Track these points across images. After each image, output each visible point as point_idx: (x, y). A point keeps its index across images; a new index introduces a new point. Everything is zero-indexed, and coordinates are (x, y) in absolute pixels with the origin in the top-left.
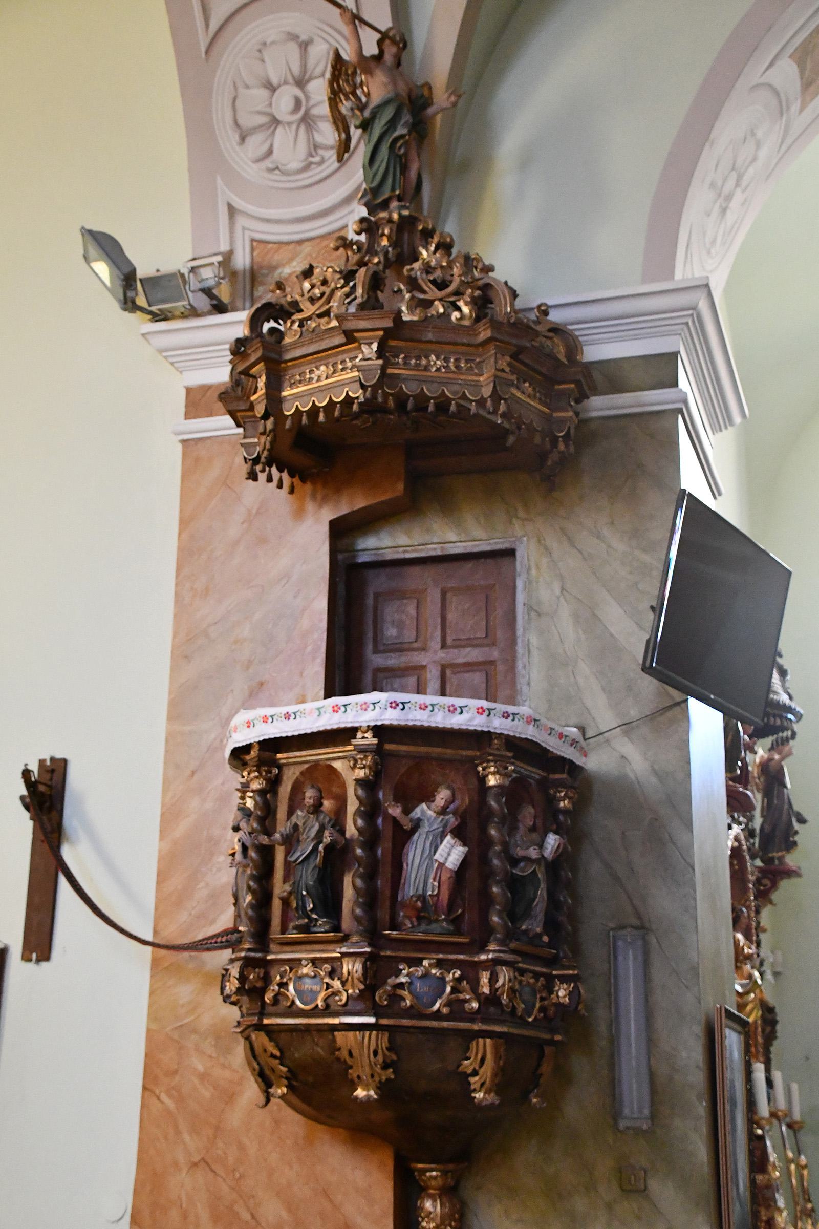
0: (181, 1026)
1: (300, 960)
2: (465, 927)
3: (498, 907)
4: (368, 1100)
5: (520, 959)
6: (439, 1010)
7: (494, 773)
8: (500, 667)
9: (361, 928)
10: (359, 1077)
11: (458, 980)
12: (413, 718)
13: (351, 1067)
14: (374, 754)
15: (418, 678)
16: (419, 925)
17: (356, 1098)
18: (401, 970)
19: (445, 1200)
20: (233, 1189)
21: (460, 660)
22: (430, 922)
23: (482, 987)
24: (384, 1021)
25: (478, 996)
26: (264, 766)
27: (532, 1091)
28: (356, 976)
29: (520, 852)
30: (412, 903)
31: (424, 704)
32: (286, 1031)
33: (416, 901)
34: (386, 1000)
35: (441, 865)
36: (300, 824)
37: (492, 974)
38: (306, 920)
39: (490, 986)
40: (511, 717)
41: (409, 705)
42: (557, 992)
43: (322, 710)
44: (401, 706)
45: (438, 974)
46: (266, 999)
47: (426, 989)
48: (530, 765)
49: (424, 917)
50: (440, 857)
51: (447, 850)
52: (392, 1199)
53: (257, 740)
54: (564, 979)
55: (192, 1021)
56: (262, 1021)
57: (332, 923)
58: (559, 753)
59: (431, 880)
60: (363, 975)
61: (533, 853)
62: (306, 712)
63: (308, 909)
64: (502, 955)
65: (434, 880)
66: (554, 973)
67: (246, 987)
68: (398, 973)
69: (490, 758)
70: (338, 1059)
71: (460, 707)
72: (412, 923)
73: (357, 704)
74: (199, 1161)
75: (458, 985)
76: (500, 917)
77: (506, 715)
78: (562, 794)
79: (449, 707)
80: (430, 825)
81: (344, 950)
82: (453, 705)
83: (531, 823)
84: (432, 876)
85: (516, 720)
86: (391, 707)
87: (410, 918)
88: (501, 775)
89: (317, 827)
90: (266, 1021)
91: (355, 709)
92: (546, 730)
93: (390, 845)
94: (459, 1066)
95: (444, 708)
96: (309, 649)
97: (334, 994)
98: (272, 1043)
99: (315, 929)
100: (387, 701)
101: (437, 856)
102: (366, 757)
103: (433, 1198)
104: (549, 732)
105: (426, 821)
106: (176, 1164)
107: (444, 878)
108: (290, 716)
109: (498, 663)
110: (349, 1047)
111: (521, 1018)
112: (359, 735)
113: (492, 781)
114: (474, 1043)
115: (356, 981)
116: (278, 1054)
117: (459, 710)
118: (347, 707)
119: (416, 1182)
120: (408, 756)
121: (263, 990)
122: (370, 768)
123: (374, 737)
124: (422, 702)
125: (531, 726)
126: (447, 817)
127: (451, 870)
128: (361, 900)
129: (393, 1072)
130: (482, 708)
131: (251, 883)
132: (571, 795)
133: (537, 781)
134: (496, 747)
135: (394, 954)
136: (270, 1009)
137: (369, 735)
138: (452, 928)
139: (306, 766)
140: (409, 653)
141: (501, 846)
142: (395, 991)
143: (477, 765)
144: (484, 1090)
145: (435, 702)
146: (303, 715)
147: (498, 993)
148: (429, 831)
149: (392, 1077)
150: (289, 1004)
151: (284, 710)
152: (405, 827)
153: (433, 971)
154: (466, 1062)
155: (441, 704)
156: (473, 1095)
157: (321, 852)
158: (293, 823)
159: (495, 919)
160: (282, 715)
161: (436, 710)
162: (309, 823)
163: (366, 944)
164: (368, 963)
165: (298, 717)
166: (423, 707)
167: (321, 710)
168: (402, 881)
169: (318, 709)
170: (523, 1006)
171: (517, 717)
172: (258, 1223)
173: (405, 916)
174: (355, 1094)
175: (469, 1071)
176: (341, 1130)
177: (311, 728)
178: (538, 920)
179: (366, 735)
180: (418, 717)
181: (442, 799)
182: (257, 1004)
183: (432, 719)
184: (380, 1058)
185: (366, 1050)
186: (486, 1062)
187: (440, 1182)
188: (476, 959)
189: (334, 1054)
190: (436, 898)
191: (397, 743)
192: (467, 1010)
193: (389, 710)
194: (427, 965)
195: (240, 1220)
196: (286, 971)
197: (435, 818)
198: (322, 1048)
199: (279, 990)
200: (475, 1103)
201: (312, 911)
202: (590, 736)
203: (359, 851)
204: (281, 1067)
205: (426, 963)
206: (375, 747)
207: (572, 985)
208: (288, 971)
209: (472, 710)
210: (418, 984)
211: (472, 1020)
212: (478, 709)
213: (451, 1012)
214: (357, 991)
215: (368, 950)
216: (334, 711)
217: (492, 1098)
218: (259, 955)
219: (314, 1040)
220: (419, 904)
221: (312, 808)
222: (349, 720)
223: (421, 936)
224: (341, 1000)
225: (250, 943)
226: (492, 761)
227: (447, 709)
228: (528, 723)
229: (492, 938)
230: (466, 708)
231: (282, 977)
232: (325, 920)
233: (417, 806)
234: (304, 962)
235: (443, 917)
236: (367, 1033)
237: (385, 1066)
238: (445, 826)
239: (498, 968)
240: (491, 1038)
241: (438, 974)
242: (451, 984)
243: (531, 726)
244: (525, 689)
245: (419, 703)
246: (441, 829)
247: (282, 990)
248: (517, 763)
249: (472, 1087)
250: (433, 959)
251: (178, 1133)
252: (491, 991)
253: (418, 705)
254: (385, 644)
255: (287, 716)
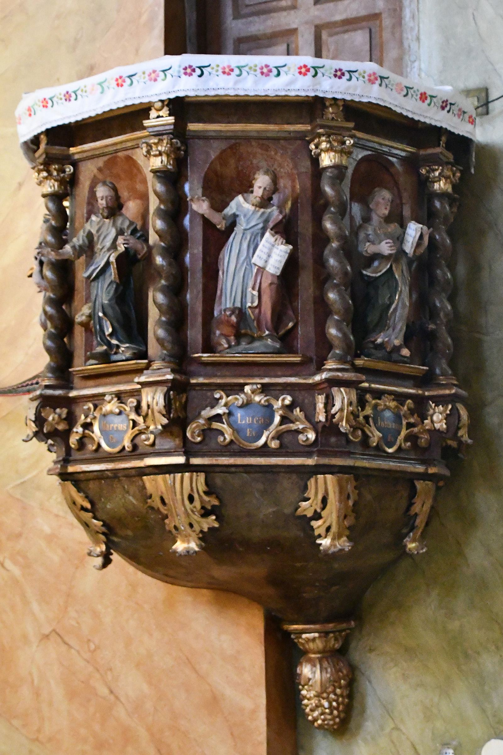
0: (22, 483)
1: (103, 395)
2: (299, 344)
3: (336, 317)
4: (188, 553)
5: (364, 378)
6: (266, 444)
7: (327, 150)
8: (387, 21)
9: (165, 352)
10: (176, 528)
11: (290, 407)
12: (215, 87)
13: (166, 517)
14: (171, 136)
15: (288, 46)
16: (238, 343)
17: (175, 552)
18: (218, 400)
19: (325, 664)
20: (88, 662)
21: (338, 17)
22: (253, 339)
23: (319, 414)
24: (195, 461)
25: (315, 426)
26: (53, 163)
27: (407, 534)
28: (156, 408)
29: (369, 249)
30: (226, 318)
31: (229, 66)
32: (94, 479)
33: (231, 315)
34: (199, 436)
35: (261, 270)
36: (94, 231)
37: (327, 398)
38: (105, 347)
39: (326, 412)
40: (347, 76)
41: (209, 69)
42: (432, 416)
43: (105, 85)
44: (198, 72)
45: (263, 402)
46: (71, 444)
47: (248, 420)
48: (378, 135)
49: (245, 335)
50: (258, 259)
51: (266, 250)
52: (263, 665)
53: (43, 129)
54: (439, 400)
55: (35, 476)
56: (67, 467)
57: (133, 349)
58: (428, 121)
59: (250, 289)
60: (165, 407)
61: (385, 248)
62: (88, 89)
63: (107, 333)
64: (340, 374)
65: (253, 289)
66: (427, 394)
67: (45, 431)
68: (215, 403)
69: (321, 131)
70: (152, 508)
71: (276, 68)
72: (229, 342)
73: (144, 73)
74: (51, 632)
75: (290, 414)
76: (339, 329)
77: (339, 73)
78: (437, 173)
79: (262, 68)
80: (248, 222)
81: (143, 379)
82: (267, 66)
83: (387, 212)
84: (251, 284)
85: (354, 79)
86: (186, 74)
87: (226, 337)
88: (335, 151)
89: (113, 233)
90: (71, 469)
91: (142, 80)
92: (399, 91)
93: (201, 249)
94: (296, 509)
95: (255, 71)
96: (145, 18)
97: (141, 433)
98: (82, 494)
99: (115, 358)
100: (180, 66)
101: (255, 260)
102: (161, 141)
103: (312, 662)
104: (405, 92)
105: (242, 217)
106: (25, 638)
107: (265, 285)
108: (70, 96)
109: (384, 16)
110: (160, 493)
111: (378, 448)
112: (153, 114)
113: (326, 160)
114: (313, 480)
115: (157, 415)
116: (89, 506)
117: (275, 72)
118: (133, 78)
119: (295, 645)
120: (219, 137)
121: (67, 433)
122: (168, 156)
123: (170, 115)
124: (226, 65)
125: (376, 86)
126: (269, 210)
127: (273, 275)
128: (163, 319)
129: (216, 520)
130: (305, 66)
131: (48, 309)
132: (449, 173)
133: (403, 160)
134: (330, 116)
135: (206, 381)
136: (76, 455)
137: (165, 112)
138: (278, 345)
139: (105, 158)
140: (275, 15)
141: (338, 241)
142: (211, 424)
143: (309, 142)
144: (331, 534)
145: (242, 64)
146: (84, 94)
147: (334, 420)
148: (245, 230)
149: (216, 525)
150: (94, 448)
151: (61, 89)
152: (218, 227)
153: (257, 398)
154: (304, 504)
155: (252, 65)
156: (318, 541)
157: (112, 262)
158: (87, 231)
159: (333, 331)
160: (62, 96)
161: (245, 74)
162: (104, 230)
163: (169, 370)
164: (172, 392)
165: (79, 97)
166: (228, 71)
167: (104, 85)
168: (219, 292)
169: (100, 84)
170: (378, 434)
171: (354, 75)
172: (117, 698)
173: (222, 334)
174: (174, 547)
175: (309, 514)
176: (204, 591)
177: (94, 110)
178: (397, 330)
179: (161, 113)
180: (222, 85)
181: (260, 187)
182: (62, 449)
183: (240, 86)
184: (197, 504)
185: (179, 496)
186: (329, 501)
187: (319, 644)
188: (311, 381)
189: (147, 503)
190: (257, 311)
191: (204, 122)
192: (301, 442)
193: (183, 76)
194: (249, 392)
195: (96, 694)
196: (89, 409)
197: (254, 213)
198: (134, 496)
199: (84, 431)
200: (320, 550)
201: (111, 335)
202: (494, 98)
203: (159, 260)
204: (95, 521)
205: (247, 389)
206: (172, 127)
207: (450, 407)
208: (92, 409)
209: (292, 70)
210: (239, 414)
211: (309, 454)
212: (300, 68)
213: (281, 445)
214: (160, 427)
215: (170, 377)
216: (118, 85)
217: (344, 544)
218: (58, 392)
219: (124, 487)
220: (234, 319)
221: (106, 211)
222: (137, 95)
223: (239, 358)
224: (148, 439)
225: (49, 378)
226: (323, 135)
227: (259, 71)
228: (372, 82)
229: (330, 355)
230: (285, 69)
231: (86, 417)
232: (127, 345)
233: (232, 199)
234: (107, 398)
235: (267, 332)
236: (179, 475)
237: (206, 513)
238: (266, 221)
239: (335, 390)
240: (332, 473)
241: (263, 402)
242: (281, 412)
243: (376, 86)
244: (414, 46)
245: (221, 66)
246: (261, 225)
247: (87, 431)
248: (360, 134)
249: (316, 533)
250: (257, 384)
251: (26, 602)
252: (327, 417)
253: (220, 70)
254: (247, 6)
255: (68, 97)
